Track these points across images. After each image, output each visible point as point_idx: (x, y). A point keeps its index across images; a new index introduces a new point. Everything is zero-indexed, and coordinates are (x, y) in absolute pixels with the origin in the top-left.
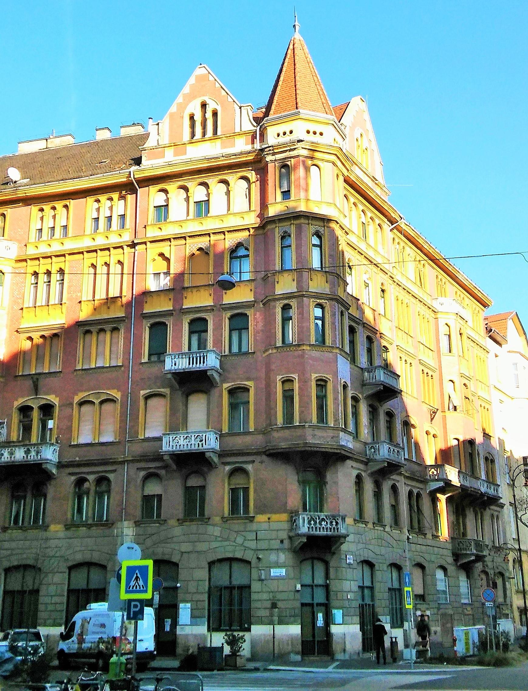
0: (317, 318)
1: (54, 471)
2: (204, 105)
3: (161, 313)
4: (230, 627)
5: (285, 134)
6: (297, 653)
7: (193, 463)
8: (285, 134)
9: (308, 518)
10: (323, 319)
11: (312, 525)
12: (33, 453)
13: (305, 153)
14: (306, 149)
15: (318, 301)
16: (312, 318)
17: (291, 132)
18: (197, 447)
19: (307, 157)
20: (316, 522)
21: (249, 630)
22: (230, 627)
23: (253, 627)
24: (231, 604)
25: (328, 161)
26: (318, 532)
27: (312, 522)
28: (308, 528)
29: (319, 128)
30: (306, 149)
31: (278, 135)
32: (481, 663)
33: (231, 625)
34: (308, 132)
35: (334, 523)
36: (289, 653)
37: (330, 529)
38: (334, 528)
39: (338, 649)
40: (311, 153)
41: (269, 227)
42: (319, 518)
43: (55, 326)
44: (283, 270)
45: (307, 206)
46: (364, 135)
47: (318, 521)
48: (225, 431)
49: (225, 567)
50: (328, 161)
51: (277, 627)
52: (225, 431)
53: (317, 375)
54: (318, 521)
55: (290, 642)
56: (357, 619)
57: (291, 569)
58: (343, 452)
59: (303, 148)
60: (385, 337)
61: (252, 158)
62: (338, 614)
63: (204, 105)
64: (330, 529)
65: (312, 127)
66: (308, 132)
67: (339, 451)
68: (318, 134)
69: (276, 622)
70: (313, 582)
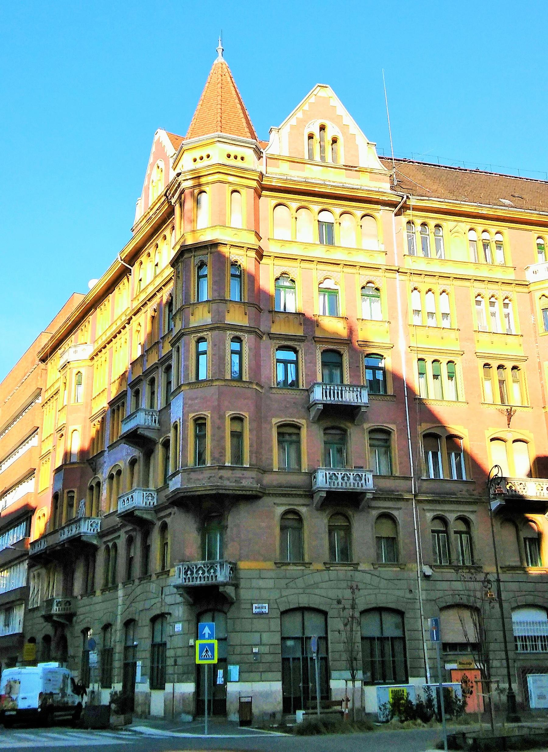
1: (95, 542)
2: (322, 128)
4: (384, 681)
6: (188, 713)
7: (343, 503)
9: (185, 568)
11: (189, 576)
12: (74, 530)
13: (190, 183)
14: (187, 180)
15: (199, 335)
18: (352, 487)
20: (193, 572)
21: (407, 682)
22: (384, 681)
23: (410, 679)
24: (383, 654)
25: (213, 183)
26: (191, 583)
27: (189, 572)
28: (185, 579)
29: (203, 152)
30: (187, 180)
32: (282, 728)
33: (384, 679)
35: (212, 571)
36: (179, 714)
37: (208, 577)
38: (212, 576)
39: (232, 710)
40: (197, 181)
42: (196, 567)
43: (498, 356)
45: (194, 237)
47: (195, 570)
48: (305, 469)
49: (297, 618)
50: (213, 183)
51: (177, 685)
52: (305, 469)
53: (193, 415)
54: (195, 570)
55: (181, 701)
56: (279, 675)
57: (186, 624)
58: (221, 492)
59: (184, 180)
61: (167, 207)
62: (234, 670)
63: (322, 128)
64: (208, 577)
65: (197, 154)
67: (214, 492)
69: (176, 680)
70: (303, 633)
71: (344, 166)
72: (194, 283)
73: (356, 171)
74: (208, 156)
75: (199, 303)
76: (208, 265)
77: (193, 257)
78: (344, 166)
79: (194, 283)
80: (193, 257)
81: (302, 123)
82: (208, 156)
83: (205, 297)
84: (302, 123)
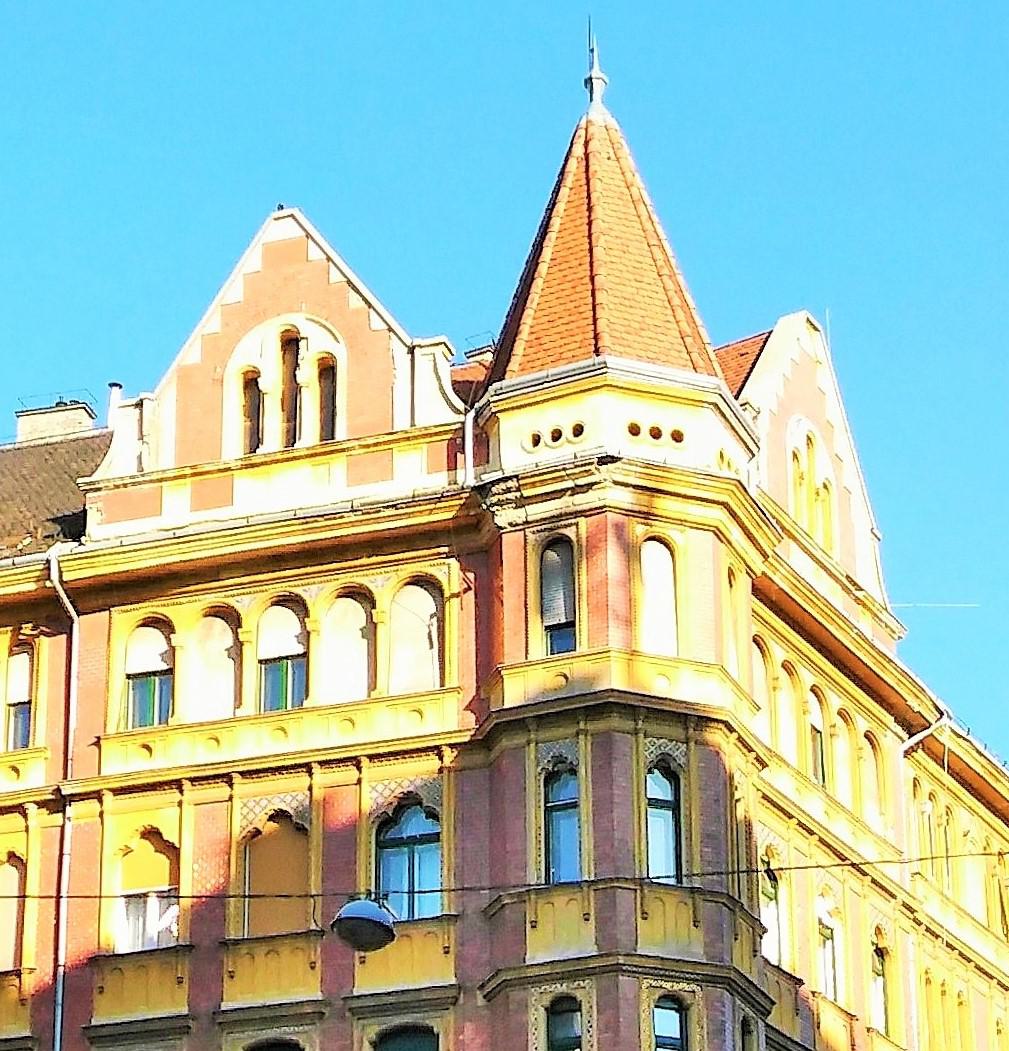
13: (625, 498)
14: (627, 485)
19: (630, 513)
29: (668, 418)
30: (627, 485)
34: (634, 430)
40: (644, 498)
45: (631, 675)
59: (616, 483)
65: (648, 414)
66: (634, 430)
71: (848, 577)
72: (368, 870)
73: (857, 600)
74: (578, 431)
75: (551, 886)
76: (582, 771)
77: (532, 745)
78: (848, 577)
79: (368, 870)
80: (532, 745)
81: (219, 349)
82: (578, 431)
83: (431, 906)
84: (219, 349)
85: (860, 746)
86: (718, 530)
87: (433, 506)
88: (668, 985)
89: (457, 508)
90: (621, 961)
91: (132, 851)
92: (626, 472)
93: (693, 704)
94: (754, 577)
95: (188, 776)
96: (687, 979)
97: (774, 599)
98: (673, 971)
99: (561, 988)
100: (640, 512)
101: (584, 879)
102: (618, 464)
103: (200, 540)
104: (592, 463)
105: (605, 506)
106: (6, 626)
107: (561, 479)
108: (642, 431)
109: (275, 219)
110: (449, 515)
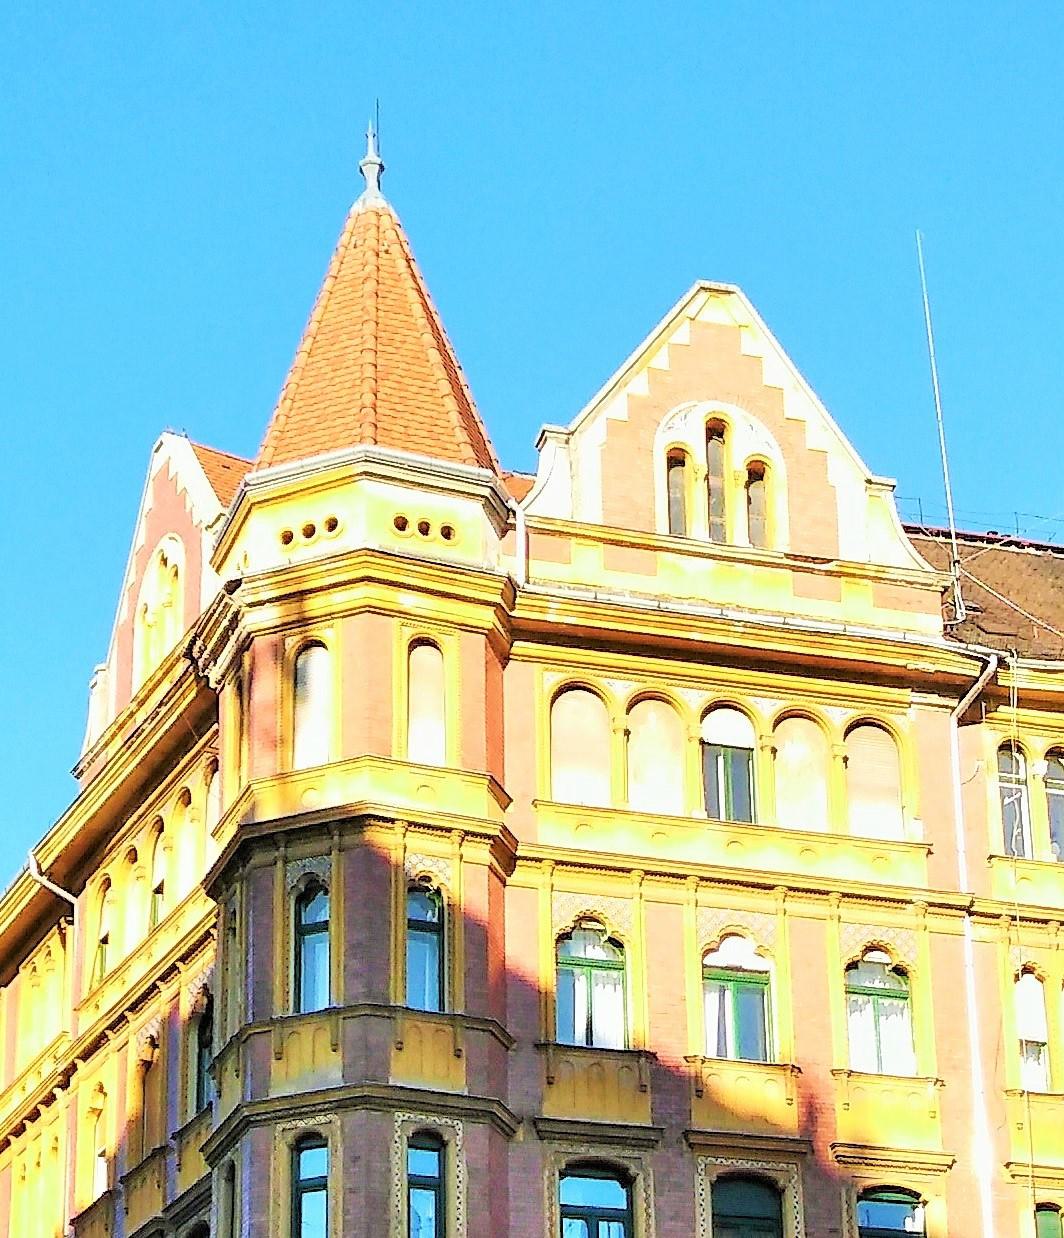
0: (416, 1182)
3: (451, 1102)
5: (310, 532)
8: (310, 532)
10: (437, 1185)
13: (272, 615)
14: (261, 603)
16: (399, 1183)
17: (332, 525)
19: (285, 626)
31: (288, 538)
34: (401, 524)
40: (293, 607)
41: (258, 858)
44: (300, 1017)
45: (284, 798)
46: (776, 475)
59: (251, 605)
60: (878, 1154)
65: (295, 515)
66: (401, 524)
68: (413, 527)
85: (764, 738)
86: (370, 606)
87: (181, 691)
88: (301, 1124)
89: (194, 684)
90: (246, 1114)
91: (101, 1110)
92: (254, 591)
93: (343, 807)
94: (486, 632)
95: (105, 1026)
96: (321, 1111)
97: (581, 635)
98: (303, 1107)
99: (432, 1120)
100: (293, 622)
101: (399, 1004)
102: (243, 586)
103: (84, 799)
104: (223, 596)
105: (249, 634)
106: (51, 928)
107: (217, 622)
108: (410, 523)
109: (156, 451)
110: (193, 694)
